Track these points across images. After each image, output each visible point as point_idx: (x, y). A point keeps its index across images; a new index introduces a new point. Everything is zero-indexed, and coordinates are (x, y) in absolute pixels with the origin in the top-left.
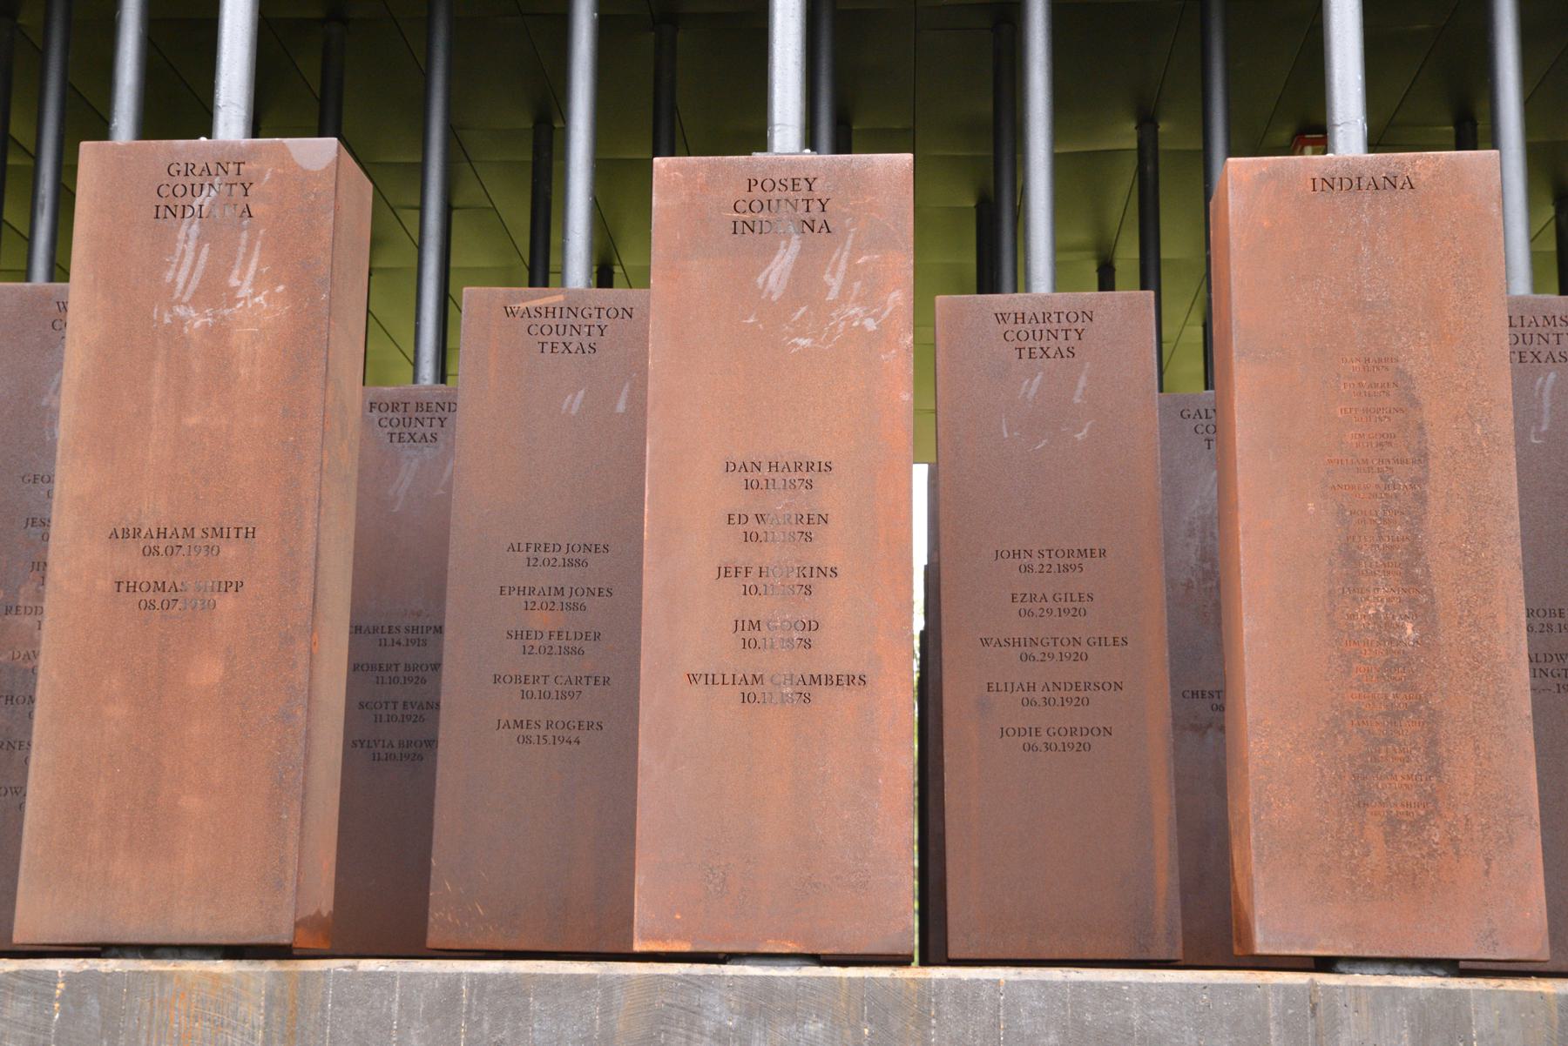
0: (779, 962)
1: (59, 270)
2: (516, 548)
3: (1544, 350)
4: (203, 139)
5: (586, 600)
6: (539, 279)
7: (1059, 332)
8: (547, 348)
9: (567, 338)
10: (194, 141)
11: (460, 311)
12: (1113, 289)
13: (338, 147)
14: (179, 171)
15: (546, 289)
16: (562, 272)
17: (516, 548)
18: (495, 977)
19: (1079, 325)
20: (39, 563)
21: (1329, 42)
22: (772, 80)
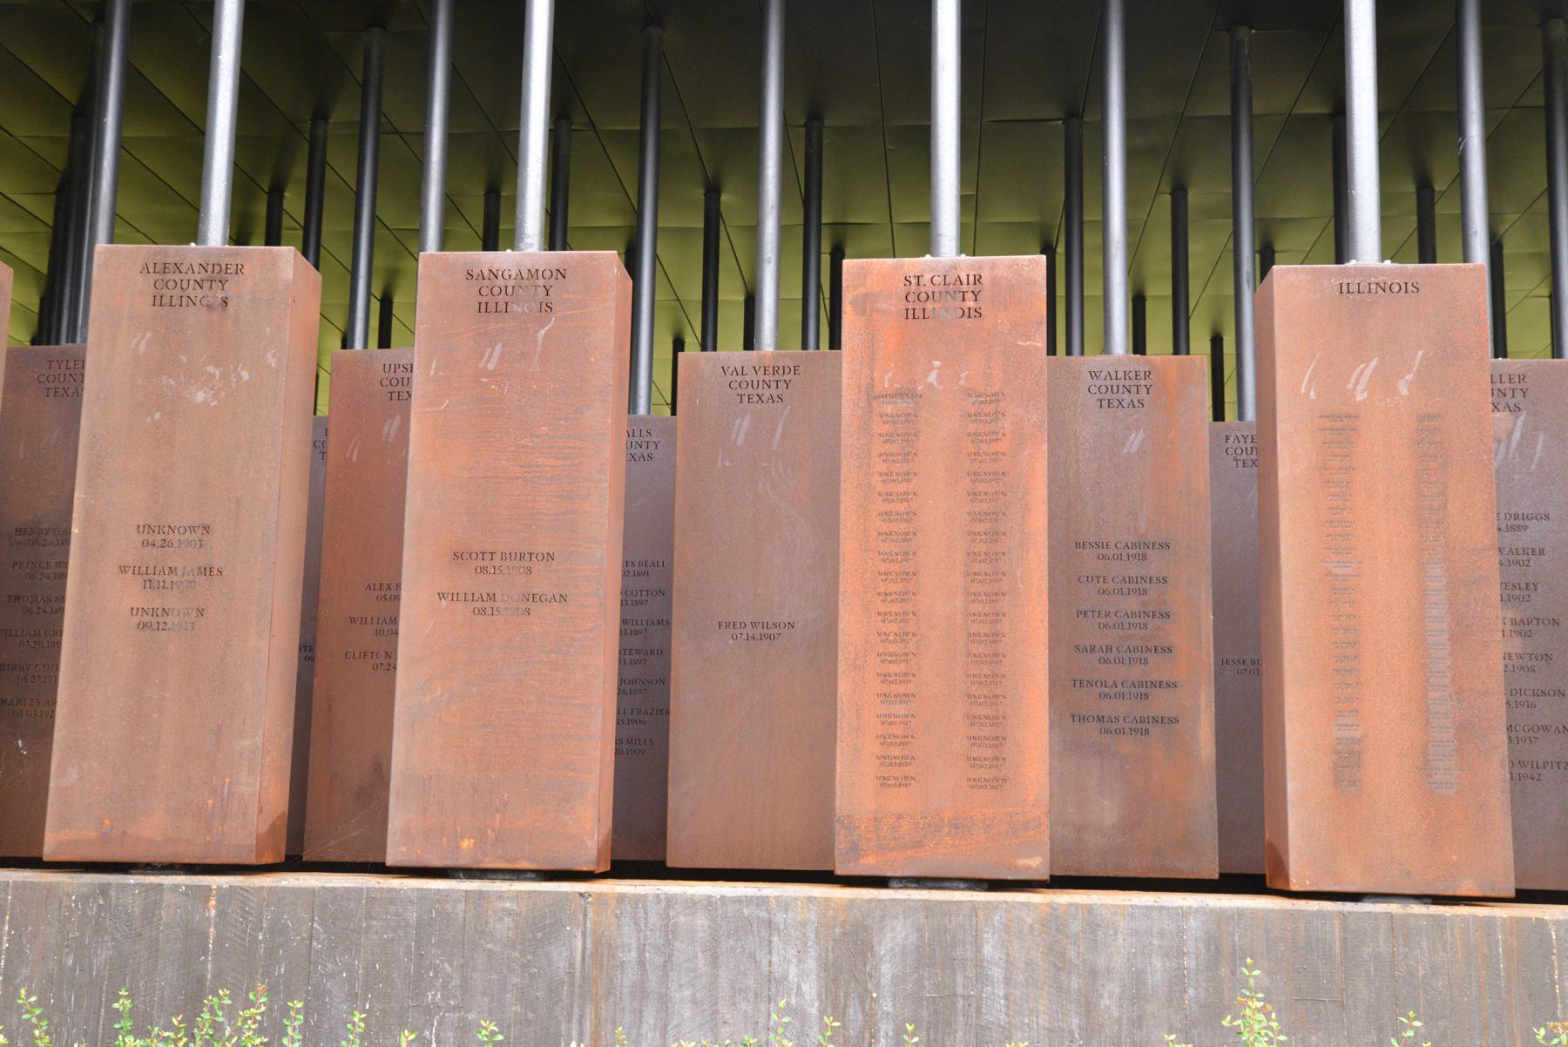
0: (1388, 900)
1: (835, 343)
2: (372, 588)
3: (1126, 397)
4: (509, 251)
5: (1147, 586)
6: (710, 345)
7: (772, 383)
8: (745, 399)
9: (760, 391)
10: (921, 258)
11: (1532, 358)
12: (752, 349)
13: (295, 252)
14: (510, 276)
15: (750, 352)
16: (760, 344)
17: (372, 588)
18: (1254, 911)
19: (787, 378)
20: (138, 609)
21: (1352, 169)
22: (228, 180)
